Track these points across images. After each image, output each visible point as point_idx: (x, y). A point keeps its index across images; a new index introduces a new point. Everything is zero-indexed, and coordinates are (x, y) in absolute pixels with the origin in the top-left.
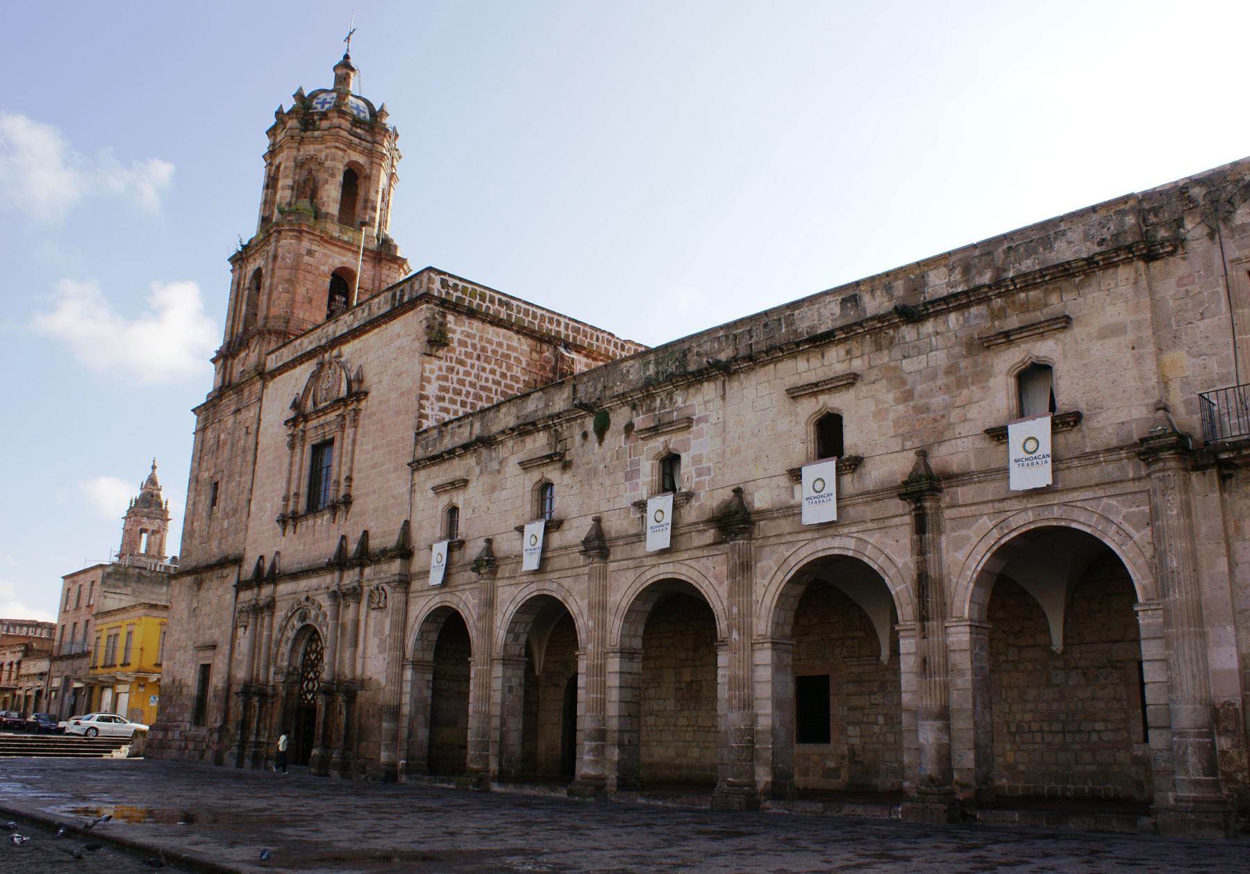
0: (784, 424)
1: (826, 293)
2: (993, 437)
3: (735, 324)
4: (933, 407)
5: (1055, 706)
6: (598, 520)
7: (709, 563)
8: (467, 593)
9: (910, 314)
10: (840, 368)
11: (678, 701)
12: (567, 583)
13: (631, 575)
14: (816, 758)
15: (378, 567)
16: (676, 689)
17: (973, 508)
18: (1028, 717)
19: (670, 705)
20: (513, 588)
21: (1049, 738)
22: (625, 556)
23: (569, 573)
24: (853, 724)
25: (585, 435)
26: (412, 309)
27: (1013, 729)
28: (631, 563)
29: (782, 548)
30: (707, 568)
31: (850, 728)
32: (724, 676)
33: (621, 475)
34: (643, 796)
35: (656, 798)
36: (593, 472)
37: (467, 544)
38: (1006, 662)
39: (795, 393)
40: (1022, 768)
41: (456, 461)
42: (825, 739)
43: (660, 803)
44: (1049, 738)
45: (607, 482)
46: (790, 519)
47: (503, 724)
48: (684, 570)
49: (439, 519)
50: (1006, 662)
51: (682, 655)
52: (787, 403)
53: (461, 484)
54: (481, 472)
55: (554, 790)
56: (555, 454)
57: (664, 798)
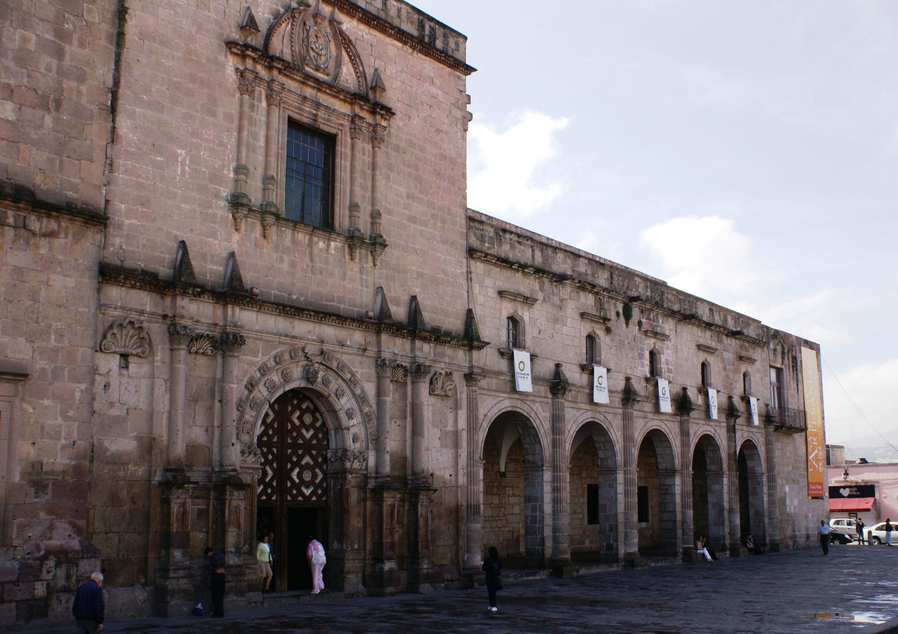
0: (695, 359)
1: (706, 301)
6: (558, 366)
8: (537, 405)
9: (734, 334)
12: (609, 417)
15: (440, 348)
20: (575, 411)
25: (618, 314)
26: (450, 66)
33: (636, 354)
36: (621, 344)
39: (699, 347)
41: (519, 275)
45: (630, 355)
47: (844, 624)
48: (663, 426)
52: (695, 348)
53: (528, 301)
55: (611, 566)
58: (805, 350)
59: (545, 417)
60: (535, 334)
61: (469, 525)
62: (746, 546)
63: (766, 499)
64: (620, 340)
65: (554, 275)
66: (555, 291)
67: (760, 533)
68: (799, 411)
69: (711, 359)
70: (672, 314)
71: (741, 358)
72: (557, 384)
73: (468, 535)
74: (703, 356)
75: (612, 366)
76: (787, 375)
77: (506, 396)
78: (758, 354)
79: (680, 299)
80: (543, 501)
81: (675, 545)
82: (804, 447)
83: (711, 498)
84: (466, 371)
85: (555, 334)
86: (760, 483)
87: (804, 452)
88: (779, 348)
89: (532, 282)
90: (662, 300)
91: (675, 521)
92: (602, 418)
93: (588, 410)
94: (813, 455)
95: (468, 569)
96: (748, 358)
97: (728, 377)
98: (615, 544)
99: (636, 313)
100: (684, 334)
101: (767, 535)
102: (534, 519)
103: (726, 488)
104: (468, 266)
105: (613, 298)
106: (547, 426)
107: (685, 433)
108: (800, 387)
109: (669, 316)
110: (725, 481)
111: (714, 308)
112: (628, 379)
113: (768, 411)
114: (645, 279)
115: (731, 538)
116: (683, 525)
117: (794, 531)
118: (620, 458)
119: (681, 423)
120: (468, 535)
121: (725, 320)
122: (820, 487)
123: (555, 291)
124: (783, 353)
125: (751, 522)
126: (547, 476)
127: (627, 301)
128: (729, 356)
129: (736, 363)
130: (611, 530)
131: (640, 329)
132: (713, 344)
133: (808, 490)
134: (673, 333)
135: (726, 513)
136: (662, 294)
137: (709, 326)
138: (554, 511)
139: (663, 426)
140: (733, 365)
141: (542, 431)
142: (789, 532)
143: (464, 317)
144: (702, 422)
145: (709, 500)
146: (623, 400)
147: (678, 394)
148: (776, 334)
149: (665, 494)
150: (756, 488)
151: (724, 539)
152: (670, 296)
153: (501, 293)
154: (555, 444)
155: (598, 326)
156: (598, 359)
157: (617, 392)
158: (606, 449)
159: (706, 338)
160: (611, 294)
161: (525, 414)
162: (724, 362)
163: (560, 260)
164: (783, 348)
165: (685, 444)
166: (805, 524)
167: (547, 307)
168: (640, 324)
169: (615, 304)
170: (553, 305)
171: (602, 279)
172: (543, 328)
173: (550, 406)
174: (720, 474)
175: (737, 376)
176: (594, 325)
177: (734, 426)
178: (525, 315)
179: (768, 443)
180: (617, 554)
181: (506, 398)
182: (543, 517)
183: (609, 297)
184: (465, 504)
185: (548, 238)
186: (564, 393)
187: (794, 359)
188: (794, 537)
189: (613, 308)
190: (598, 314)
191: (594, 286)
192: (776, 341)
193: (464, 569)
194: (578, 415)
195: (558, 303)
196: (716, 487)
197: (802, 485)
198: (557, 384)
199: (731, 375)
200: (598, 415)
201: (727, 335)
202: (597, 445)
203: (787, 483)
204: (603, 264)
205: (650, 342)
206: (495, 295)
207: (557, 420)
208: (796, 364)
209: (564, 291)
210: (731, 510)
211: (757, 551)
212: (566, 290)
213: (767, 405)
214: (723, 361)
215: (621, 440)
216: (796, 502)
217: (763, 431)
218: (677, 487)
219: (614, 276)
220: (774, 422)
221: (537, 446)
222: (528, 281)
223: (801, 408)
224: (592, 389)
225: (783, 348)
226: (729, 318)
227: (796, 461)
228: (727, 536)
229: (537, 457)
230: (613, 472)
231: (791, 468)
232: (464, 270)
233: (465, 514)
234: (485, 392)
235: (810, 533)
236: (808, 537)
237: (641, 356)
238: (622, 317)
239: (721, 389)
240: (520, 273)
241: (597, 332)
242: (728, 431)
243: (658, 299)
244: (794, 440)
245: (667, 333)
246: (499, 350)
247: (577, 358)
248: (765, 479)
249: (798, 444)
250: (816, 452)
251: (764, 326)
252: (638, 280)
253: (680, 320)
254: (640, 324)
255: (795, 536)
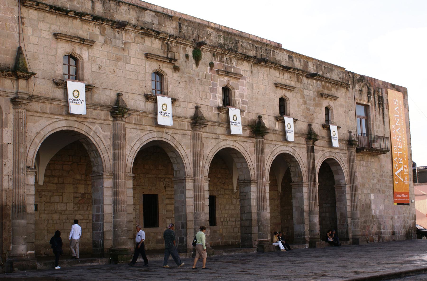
0: (272, 95)
2: (175, 99)
3: (324, 63)
4: (311, 110)
5: (233, 212)
6: (119, 95)
7: (247, 145)
8: (97, 125)
9: (312, 76)
10: (288, 82)
11: (76, 204)
12: (178, 137)
13: (213, 142)
14: (153, 235)
16: (75, 197)
17: (319, 147)
18: (226, 215)
19: (70, 207)
20: (139, 132)
21: (232, 223)
22: (210, 131)
23: (179, 132)
24: (169, 218)
25: (187, 56)
27: (222, 220)
28: (214, 136)
29: (272, 146)
30: (247, 147)
31: (168, 220)
32: (253, 196)
33: (207, 88)
34: (225, 252)
35: (231, 251)
36: (191, 80)
37: (95, 90)
38: (220, 194)
39: (276, 85)
40: (224, 234)
41: (78, 22)
42: (158, 226)
43: (233, 254)
44: (232, 223)
45: (200, 89)
46: (274, 135)
48: (238, 145)
49: (291, 107)
50: (220, 194)
51: (78, 177)
52: (273, 87)
54: (106, 42)
56: (167, 58)
57: (234, 251)
58: (391, 93)
59: (105, 136)
60: (95, 68)
61: (14, 221)
62: (327, 241)
63: (348, 203)
64: (190, 77)
65: (114, 22)
66: (117, 35)
67: (345, 230)
68: (385, 138)
69: (288, 95)
70: (246, 58)
71: (322, 95)
72: (257, 129)
73: (13, 230)
74: (280, 93)
75: (180, 96)
76: (374, 111)
77: (62, 118)
78: (341, 93)
79: (256, 47)
80: (103, 203)
81: (251, 238)
82: (391, 165)
83: (295, 203)
84: (13, 96)
85: (117, 70)
86: (344, 192)
87: (391, 169)
88: (365, 90)
89: (91, 28)
90: (237, 48)
91: (251, 220)
92: (169, 137)
93: (154, 131)
94: (399, 171)
95: (12, 257)
96: (328, 95)
97: (308, 109)
98: (185, 237)
99: (206, 57)
100: (261, 75)
101: (350, 232)
102: (98, 216)
103: (307, 196)
104: (20, 12)
105: (181, 44)
106: (108, 142)
107: (260, 152)
108: (386, 119)
109: (244, 60)
110: (305, 189)
111: (293, 55)
112: (197, 108)
113: (350, 136)
114: (218, 30)
115: (310, 234)
116: (258, 223)
117: (379, 228)
118: (189, 170)
119: (257, 144)
120: (13, 230)
121: (306, 65)
122: (406, 196)
123: (117, 35)
124: (369, 93)
125: (338, 222)
126: (108, 183)
127: (195, 46)
128: (310, 93)
129: (317, 99)
130: (182, 227)
131: (211, 69)
132: (293, 84)
133: (394, 197)
134: (249, 73)
135: (306, 215)
136: (237, 42)
137: (286, 69)
138: (114, 211)
139: (238, 145)
140: (314, 99)
141: (102, 147)
142: (374, 229)
143: (16, 53)
144: (280, 143)
145: (294, 204)
146: (192, 124)
147: (253, 121)
148: (362, 79)
149: (244, 199)
150: (340, 196)
151: (305, 235)
152: (245, 45)
153: (56, 35)
154: (195, 164)
155: (165, 65)
156: (165, 91)
157: (186, 117)
158: (178, 163)
159: (285, 78)
160: (180, 40)
161: (291, 154)
162: (304, 97)
163: (123, 12)
164: (369, 89)
165: (260, 160)
166: (391, 223)
167: (107, 49)
168: (211, 65)
169: (184, 49)
170: (115, 47)
171: (170, 28)
172: (103, 65)
173: (111, 127)
174: (301, 184)
175: (318, 109)
176: (161, 64)
177: (313, 147)
178: (84, 53)
179: (350, 161)
180: (186, 245)
181: (63, 120)
182: (103, 215)
183: (177, 43)
184: (11, 204)
185: (163, 8)
186: (123, 116)
187: (381, 99)
188: (379, 234)
189: (181, 51)
190: (166, 56)
191: (158, 33)
192: (362, 84)
193: (9, 257)
194: (142, 135)
195: (121, 45)
196: (298, 195)
197: (388, 194)
198: (310, 136)
199: (312, 108)
200: (164, 136)
201: (307, 77)
202: (172, 161)
203: (372, 193)
204: (171, 17)
205: (224, 80)
206: (51, 37)
207: (117, 140)
208: (381, 102)
209: (127, 36)
210: (310, 212)
211: (335, 244)
212: (130, 36)
213: (350, 132)
214: (303, 96)
215: (190, 156)
216: (381, 207)
217: (347, 152)
218: (252, 194)
219: (183, 26)
220: (355, 144)
221: (99, 159)
222: (87, 27)
223: (387, 135)
224: (156, 114)
225: (369, 89)
226: (310, 64)
227: (382, 176)
228: (307, 232)
229: (100, 167)
230: (183, 181)
231: (376, 181)
232: (16, 16)
233: (11, 212)
234: (38, 115)
235: (396, 230)
236: (394, 233)
237: (213, 90)
238: (191, 59)
239: (300, 118)
240: (78, 20)
241: (164, 70)
242: (308, 151)
243: (231, 46)
244: (380, 160)
245: (242, 73)
246: (53, 80)
247: (142, 89)
248: (348, 189)
249: (383, 162)
250: (402, 169)
251: (349, 72)
252: (210, 31)
253: (255, 64)
254: (211, 65)
255: (381, 233)
